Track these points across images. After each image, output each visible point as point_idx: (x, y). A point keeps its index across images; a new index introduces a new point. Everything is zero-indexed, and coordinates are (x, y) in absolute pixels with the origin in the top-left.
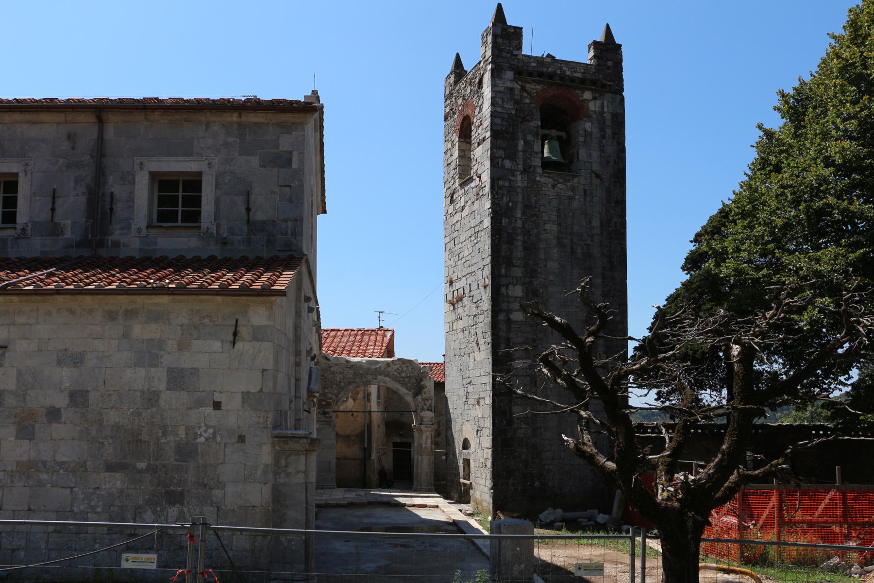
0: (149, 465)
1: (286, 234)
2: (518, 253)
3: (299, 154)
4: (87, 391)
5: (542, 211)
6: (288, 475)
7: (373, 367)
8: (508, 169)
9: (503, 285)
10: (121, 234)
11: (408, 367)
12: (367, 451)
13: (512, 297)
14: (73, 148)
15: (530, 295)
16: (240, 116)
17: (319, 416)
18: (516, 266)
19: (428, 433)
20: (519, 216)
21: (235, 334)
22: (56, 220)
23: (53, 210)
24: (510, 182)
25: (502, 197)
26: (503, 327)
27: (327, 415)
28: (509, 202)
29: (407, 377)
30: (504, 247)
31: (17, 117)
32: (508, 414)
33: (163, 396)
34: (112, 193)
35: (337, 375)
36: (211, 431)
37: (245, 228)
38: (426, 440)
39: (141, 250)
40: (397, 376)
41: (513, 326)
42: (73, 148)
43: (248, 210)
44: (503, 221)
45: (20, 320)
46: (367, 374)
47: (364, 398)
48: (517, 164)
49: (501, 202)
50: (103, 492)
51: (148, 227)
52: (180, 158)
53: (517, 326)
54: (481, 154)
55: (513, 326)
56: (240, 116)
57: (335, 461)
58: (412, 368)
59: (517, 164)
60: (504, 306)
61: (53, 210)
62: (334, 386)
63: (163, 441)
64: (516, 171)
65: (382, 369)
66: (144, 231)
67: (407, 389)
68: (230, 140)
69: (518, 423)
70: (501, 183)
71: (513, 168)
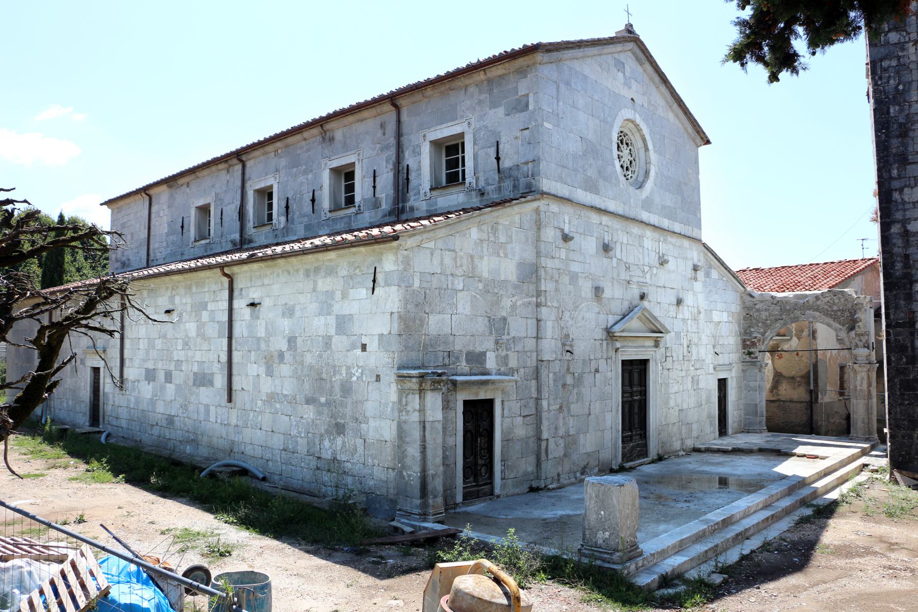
0: (327, 400)
1: (528, 177)
3: (534, 94)
4: (296, 337)
6: (408, 412)
7: (802, 302)
8: (896, 44)
9: (896, 190)
10: (414, 200)
11: (840, 298)
12: (813, 394)
14: (384, 134)
16: (485, 73)
17: (744, 356)
19: (863, 374)
21: (374, 281)
22: (376, 196)
23: (374, 187)
24: (899, 60)
25: (888, 82)
26: (899, 242)
29: (839, 310)
30: (895, 142)
31: (351, 118)
32: (909, 349)
33: (334, 340)
34: (408, 165)
36: (360, 371)
37: (497, 177)
38: (862, 383)
39: (427, 210)
40: (827, 310)
41: (911, 239)
42: (384, 134)
43: (498, 159)
44: (892, 111)
45: (266, 282)
46: (795, 309)
47: (809, 335)
48: (908, 34)
49: (886, 88)
50: (304, 421)
51: (431, 189)
52: (449, 124)
55: (911, 239)
56: (485, 73)
57: (764, 403)
58: (845, 300)
59: (908, 34)
60: (898, 216)
61: (374, 187)
62: (760, 325)
63: (334, 379)
64: (907, 42)
65: (811, 303)
66: (428, 194)
67: (840, 323)
68: (482, 97)
70: (885, 64)
71: (902, 40)
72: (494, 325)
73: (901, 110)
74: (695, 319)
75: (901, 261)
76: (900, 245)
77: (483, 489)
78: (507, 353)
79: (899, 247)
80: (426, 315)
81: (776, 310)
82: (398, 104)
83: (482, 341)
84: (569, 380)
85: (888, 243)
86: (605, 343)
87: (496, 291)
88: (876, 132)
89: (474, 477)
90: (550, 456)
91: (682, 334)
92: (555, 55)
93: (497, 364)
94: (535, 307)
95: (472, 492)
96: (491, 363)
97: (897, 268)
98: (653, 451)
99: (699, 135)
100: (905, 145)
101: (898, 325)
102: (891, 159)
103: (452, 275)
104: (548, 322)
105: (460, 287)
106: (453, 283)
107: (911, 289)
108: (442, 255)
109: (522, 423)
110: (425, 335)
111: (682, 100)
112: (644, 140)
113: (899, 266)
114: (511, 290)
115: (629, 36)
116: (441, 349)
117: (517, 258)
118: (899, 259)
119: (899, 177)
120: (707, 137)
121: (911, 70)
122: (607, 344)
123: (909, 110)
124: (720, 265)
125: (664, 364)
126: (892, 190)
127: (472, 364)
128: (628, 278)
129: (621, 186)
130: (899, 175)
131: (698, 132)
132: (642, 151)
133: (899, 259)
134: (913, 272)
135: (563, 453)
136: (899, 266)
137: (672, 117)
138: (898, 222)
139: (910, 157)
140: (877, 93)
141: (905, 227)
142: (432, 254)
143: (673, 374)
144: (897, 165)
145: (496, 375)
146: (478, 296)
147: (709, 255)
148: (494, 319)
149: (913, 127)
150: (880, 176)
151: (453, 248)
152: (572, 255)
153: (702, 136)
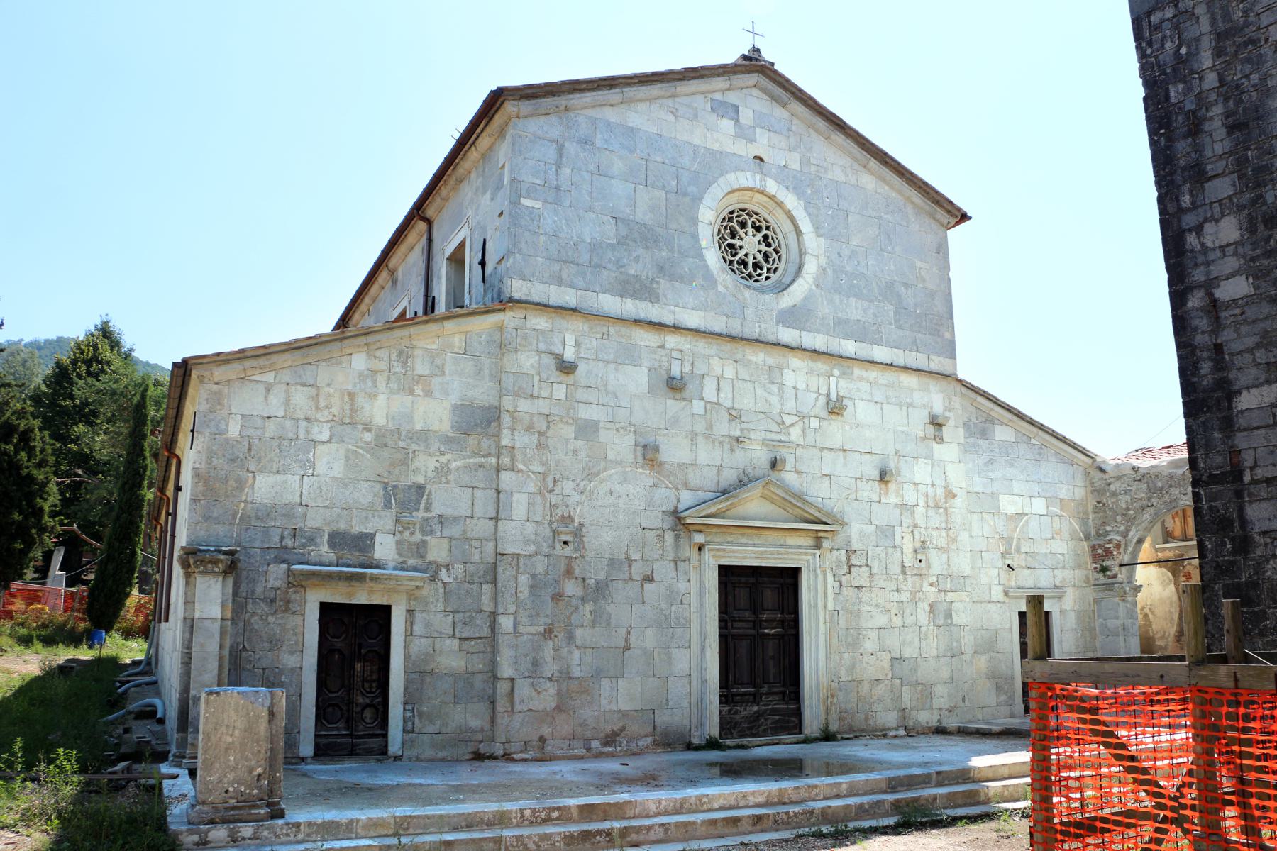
2: (1217, 141)
5: (1265, 23)
9: (1190, 230)
13: (1214, 249)
15: (1261, 228)
18: (1217, 176)
20: (1208, 63)
25: (1163, 45)
26: (1202, 323)
27: (1108, 573)
28: (1179, 47)
30: (1182, 146)
32: (1236, 524)
34: (434, 297)
35: (1120, 497)
44: (1172, 94)
46: (1171, 486)
53: (1237, 311)
54: (497, 105)
60: (1198, 275)
62: (1119, 518)
69: (1266, 545)
72: (395, 495)
73: (1188, 89)
74: (937, 506)
75: (1209, 358)
76: (1205, 329)
77: (365, 743)
78: (424, 538)
79: (1203, 333)
80: (251, 475)
81: (1141, 490)
82: (428, 216)
83: (367, 518)
84: (571, 588)
85: (1184, 328)
86: (669, 537)
87: (402, 444)
88: (1150, 135)
89: (347, 722)
90: (518, 707)
91: (898, 531)
92: (562, 101)
93: (400, 555)
94: (493, 471)
95: (340, 744)
96: (385, 549)
97: (1203, 372)
98: (812, 720)
99: (941, 206)
100: (1198, 148)
101: (1214, 479)
102: (1178, 178)
103: (307, 419)
104: (516, 496)
105: (325, 436)
106: (308, 432)
107: (1230, 408)
108: (287, 392)
109: (457, 648)
110: (246, 502)
111: (886, 154)
112: (792, 220)
113: (1206, 367)
114: (435, 445)
115: (753, 64)
116: (277, 524)
117: (454, 398)
118: (1205, 355)
119: (1194, 206)
120: (959, 209)
121: (1198, 18)
122: (677, 537)
123: (1200, 86)
124: (1015, 418)
125: (844, 579)
126: (1184, 231)
127: (343, 550)
128: (738, 433)
129: (721, 288)
130: (1192, 203)
131: (937, 203)
132: (792, 237)
133: (1205, 355)
134: (1232, 375)
135: (553, 705)
136: (1206, 367)
137: (870, 181)
138: (1199, 287)
139: (1209, 167)
140: (1147, 70)
141: (1211, 294)
142: (268, 390)
143: (876, 597)
144: (1188, 185)
145: (395, 569)
146: (361, 451)
147: (980, 399)
148: (395, 487)
149: (1210, 114)
150: (1163, 211)
151: (311, 382)
152: (581, 394)
153: (950, 208)
